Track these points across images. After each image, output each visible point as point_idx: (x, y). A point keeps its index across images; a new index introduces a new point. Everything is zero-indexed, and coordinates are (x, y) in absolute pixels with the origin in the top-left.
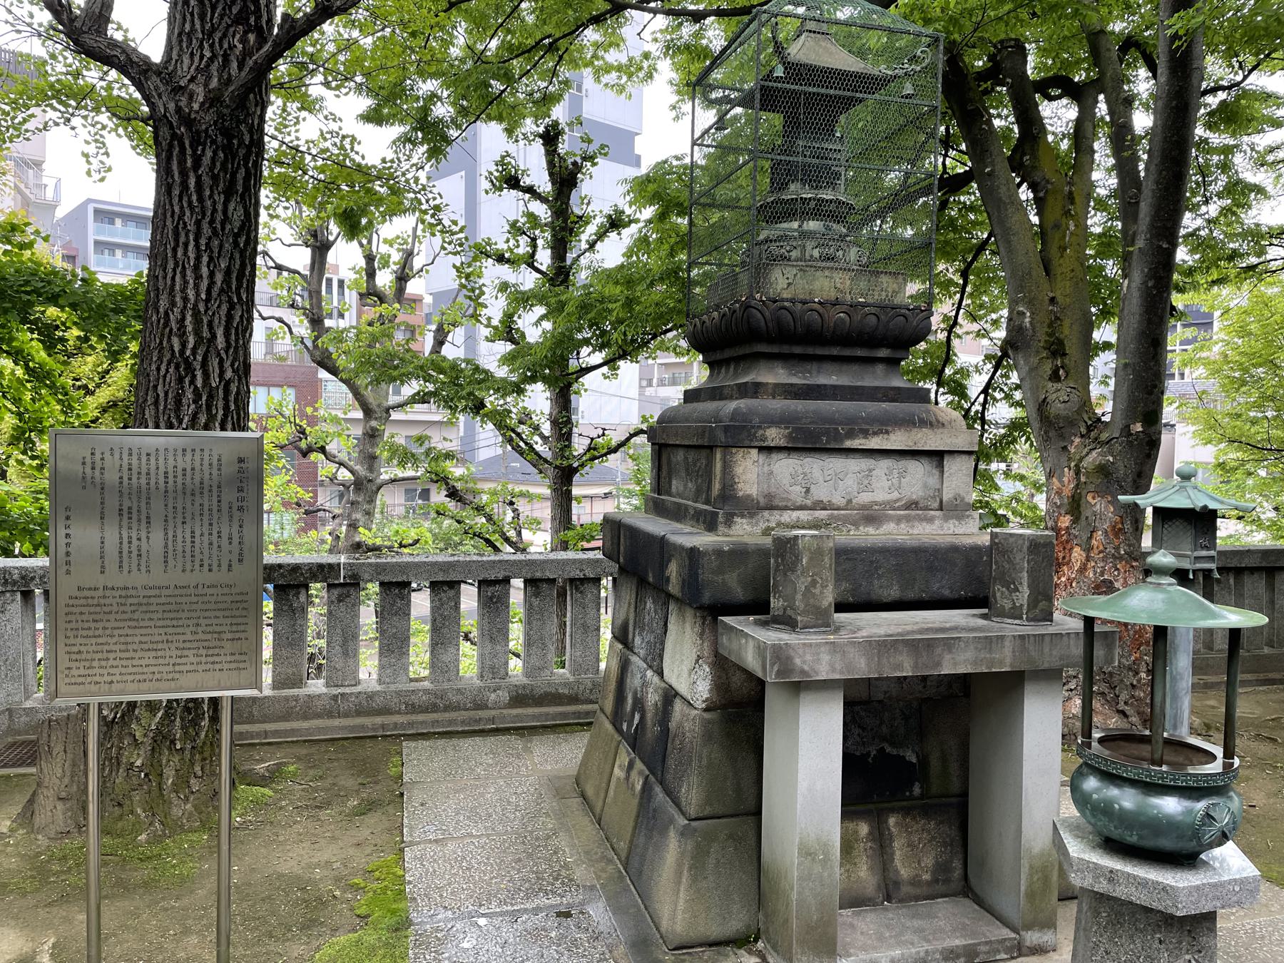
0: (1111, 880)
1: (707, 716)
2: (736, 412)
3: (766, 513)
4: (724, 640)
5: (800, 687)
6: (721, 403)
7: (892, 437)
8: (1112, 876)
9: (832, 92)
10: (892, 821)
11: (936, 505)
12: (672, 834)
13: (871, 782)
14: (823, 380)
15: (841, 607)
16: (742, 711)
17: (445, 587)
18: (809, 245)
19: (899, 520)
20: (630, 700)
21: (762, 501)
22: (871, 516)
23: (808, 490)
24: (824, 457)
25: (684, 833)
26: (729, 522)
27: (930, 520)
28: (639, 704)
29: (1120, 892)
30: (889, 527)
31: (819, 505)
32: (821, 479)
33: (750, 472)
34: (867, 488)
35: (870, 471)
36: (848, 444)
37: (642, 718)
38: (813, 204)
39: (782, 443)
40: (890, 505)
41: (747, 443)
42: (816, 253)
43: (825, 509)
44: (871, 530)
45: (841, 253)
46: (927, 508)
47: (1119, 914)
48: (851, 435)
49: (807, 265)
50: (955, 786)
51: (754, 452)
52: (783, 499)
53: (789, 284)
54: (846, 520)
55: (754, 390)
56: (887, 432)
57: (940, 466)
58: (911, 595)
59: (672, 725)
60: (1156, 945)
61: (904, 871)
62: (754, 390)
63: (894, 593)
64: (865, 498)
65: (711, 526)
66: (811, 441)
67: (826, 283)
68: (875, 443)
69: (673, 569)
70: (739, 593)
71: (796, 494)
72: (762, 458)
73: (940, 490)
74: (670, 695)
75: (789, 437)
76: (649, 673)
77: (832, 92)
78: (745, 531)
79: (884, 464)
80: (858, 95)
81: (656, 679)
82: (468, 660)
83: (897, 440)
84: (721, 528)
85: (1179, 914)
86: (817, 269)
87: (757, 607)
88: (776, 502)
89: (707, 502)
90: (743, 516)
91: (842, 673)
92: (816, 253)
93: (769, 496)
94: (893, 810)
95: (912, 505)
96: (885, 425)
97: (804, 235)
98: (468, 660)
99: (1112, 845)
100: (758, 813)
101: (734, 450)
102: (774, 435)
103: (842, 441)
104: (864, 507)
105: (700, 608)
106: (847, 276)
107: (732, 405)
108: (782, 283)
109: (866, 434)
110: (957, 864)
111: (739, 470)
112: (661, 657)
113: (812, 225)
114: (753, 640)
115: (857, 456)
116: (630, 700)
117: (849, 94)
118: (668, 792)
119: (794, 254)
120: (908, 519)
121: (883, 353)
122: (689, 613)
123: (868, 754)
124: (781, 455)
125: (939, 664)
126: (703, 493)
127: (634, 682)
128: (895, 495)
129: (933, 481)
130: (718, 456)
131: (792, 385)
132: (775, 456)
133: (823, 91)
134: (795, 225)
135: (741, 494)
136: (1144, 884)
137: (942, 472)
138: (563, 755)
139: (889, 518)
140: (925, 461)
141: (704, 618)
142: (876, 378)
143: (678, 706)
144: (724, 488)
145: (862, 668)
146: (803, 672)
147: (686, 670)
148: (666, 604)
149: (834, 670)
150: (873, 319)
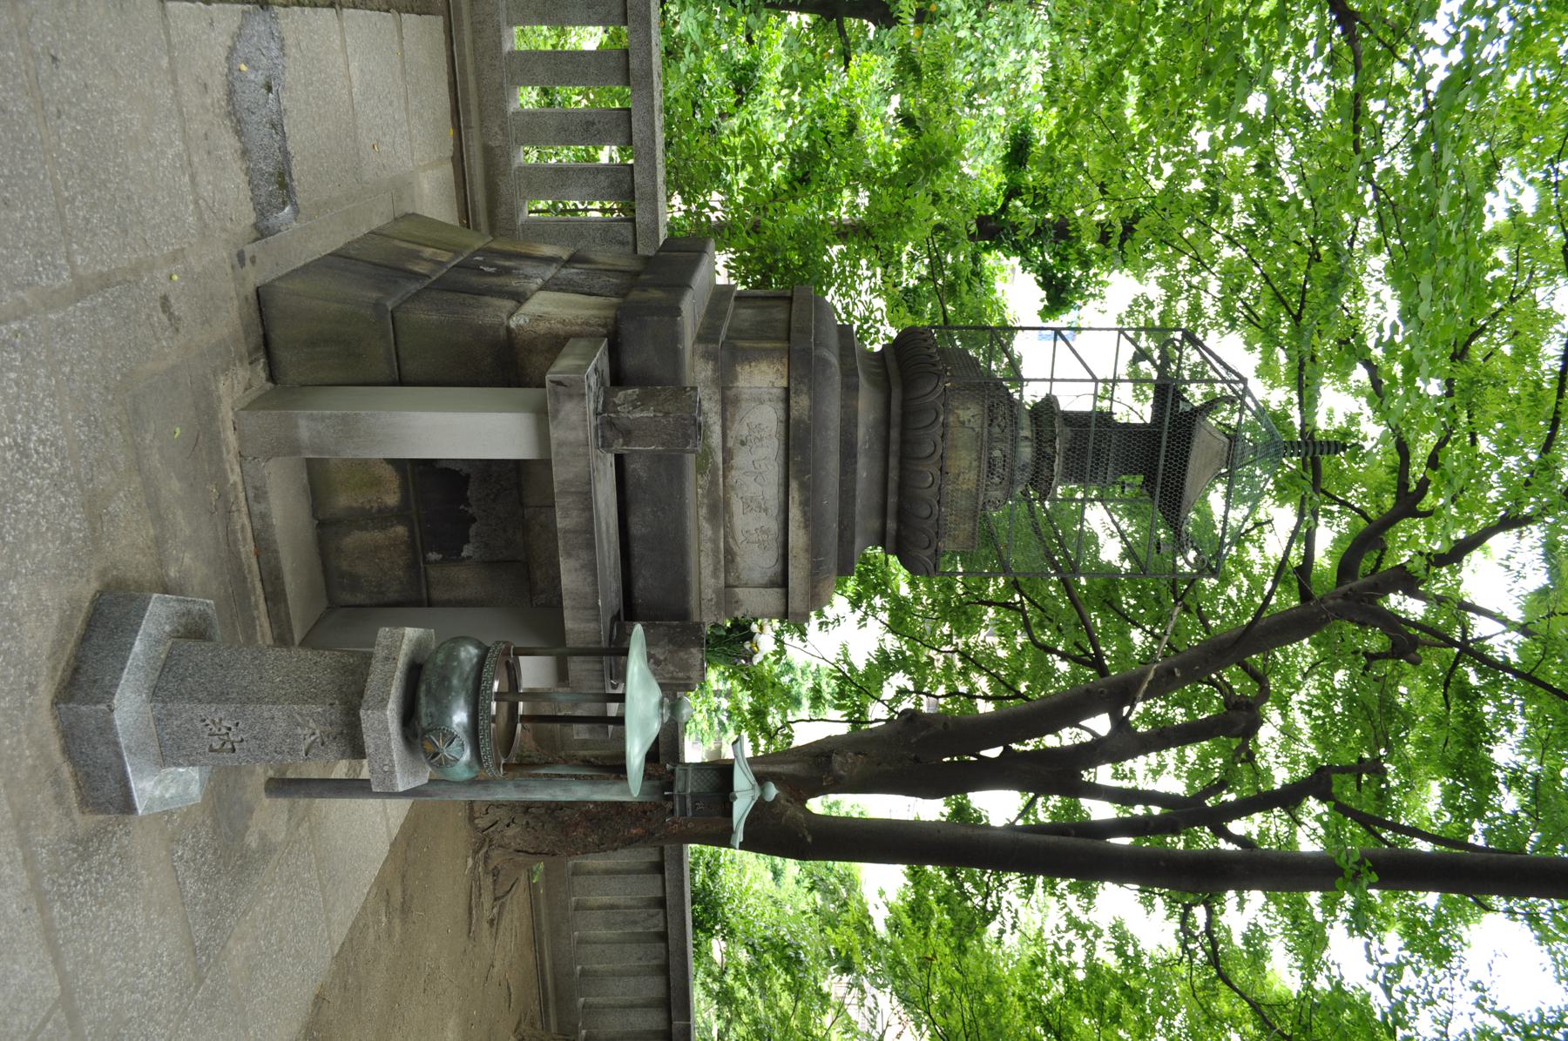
0: (387, 659)
1: (503, 332)
2: (825, 363)
3: (718, 397)
4: (583, 343)
5: (542, 418)
6: (836, 351)
7: (801, 532)
8: (390, 659)
9: (1162, 462)
10: (401, 530)
11: (731, 581)
12: (375, 295)
13: (441, 489)
14: (862, 461)
15: (620, 459)
16: (506, 366)
17: (621, 126)
18: (1007, 447)
19: (715, 541)
20: (507, 263)
21: (731, 393)
22: (719, 510)
23: (743, 443)
24: (781, 459)
25: (377, 305)
26: (707, 356)
27: (715, 574)
28: (507, 271)
29: (377, 667)
30: (707, 530)
31: (728, 455)
32: (754, 457)
33: (762, 379)
34: (747, 505)
35: (766, 510)
36: (794, 485)
37: (490, 274)
38: (1049, 450)
39: (794, 413)
40: (729, 534)
41: (793, 374)
42: (997, 453)
43: (724, 462)
44: (703, 511)
45: (997, 480)
46: (727, 572)
47: (353, 673)
48: (803, 487)
49: (984, 444)
50: (436, 594)
51: (784, 383)
52: (733, 416)
53: (963, 423)
54: (714, 483)
55: (850, 389)
56: (806, 527)
57: (771, 584)
58: (637, 549)
59: (488, 299)
60: (328, 701)
61: (354, 540)
62: (850, 389)
63: (637, 528)
64: (737, 506)
65: (701, 338)
66: (796, 442)
67: (964, 463)
68: (795, 513)
69: (656, 294)
70: (631, 361)
71: (740, 430)
72: (778, 392)
73: (746, 585)
74: (520, 298)
75: (799, 421)
76: (539, 281)
77: (1162, 462)
78: (699, 372)
79: (774, 526)
80: (1158, 490)
81: (534, 287)
82: (528, 97)
83: (798, 538)
84: (701, 348)
85: (362, 713)
86: (980, 453)
87: (618, 378)
88: (730, 409)
89: (728, 337)
90: (714, 371)
91: (557, 454)
92: (997, 453)
93: (736, 401)
94: (411, 531)
95: (730, 556)
96: (813, 522)
97: (1015, 441)
98: (528, 97)
99: (415, 671)
100: (401, 382)
101: (785, 361)
102: (801, 404)
103: (796, 478)
104: (727, 504)
105: (616, 320)
106: (971, 485)
107: (834, 360)
108: (964, 415)
109: (805, 504)
110: (361, 598)
111: (764, 366)
112: (559, 290)
113: (1026, 452)
114: (585, 367)
115: (782, 496)
116: (507, 263)
117: (1159, 480)
118: (417, 294)
119: (996, 430)
120: (716, 551)
121: (891, 525)
122: (611, 313)
123: (469, 505)
124: (781, 413)
125: (569, 555)
126: (737, 334)
127: (528, 268)
128: (740, 538)
129: (757, 576)
130: (778, 345)
131: (856, 426)
132: (781, 405)
133: (1163, 452)
134: (1026, 433)
135: (739, 369)
136: (387, 684)
137: (766, 586)
138: (432, 196)
139: (715, 530)
140: (778, 568)
141: (605, 326)
142: (865, 522)
143: (509, 304)
144: (743, 349)
145: (561, 473)
146: (557, 411)
147: (545, 308)
148: (617, 295)
149: (560, 445)
150: (926, 513)
